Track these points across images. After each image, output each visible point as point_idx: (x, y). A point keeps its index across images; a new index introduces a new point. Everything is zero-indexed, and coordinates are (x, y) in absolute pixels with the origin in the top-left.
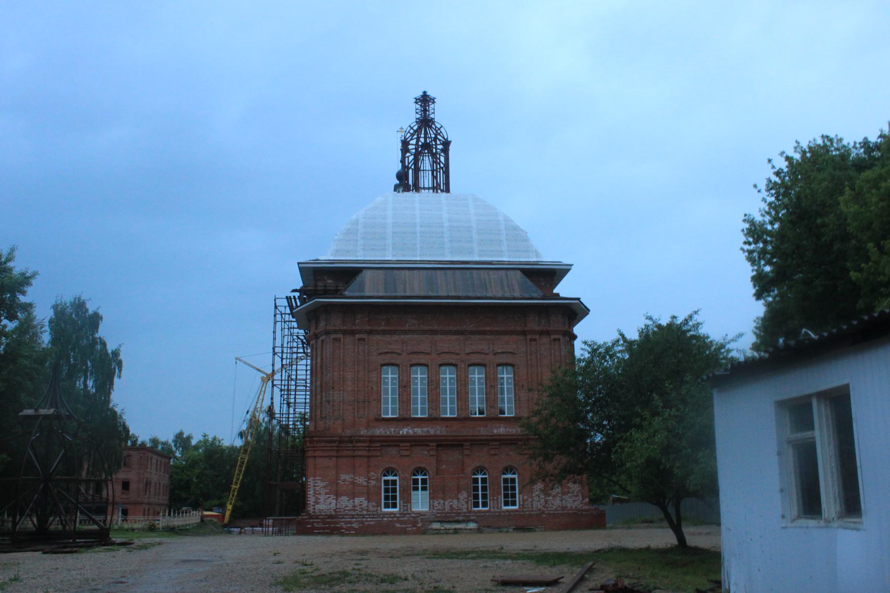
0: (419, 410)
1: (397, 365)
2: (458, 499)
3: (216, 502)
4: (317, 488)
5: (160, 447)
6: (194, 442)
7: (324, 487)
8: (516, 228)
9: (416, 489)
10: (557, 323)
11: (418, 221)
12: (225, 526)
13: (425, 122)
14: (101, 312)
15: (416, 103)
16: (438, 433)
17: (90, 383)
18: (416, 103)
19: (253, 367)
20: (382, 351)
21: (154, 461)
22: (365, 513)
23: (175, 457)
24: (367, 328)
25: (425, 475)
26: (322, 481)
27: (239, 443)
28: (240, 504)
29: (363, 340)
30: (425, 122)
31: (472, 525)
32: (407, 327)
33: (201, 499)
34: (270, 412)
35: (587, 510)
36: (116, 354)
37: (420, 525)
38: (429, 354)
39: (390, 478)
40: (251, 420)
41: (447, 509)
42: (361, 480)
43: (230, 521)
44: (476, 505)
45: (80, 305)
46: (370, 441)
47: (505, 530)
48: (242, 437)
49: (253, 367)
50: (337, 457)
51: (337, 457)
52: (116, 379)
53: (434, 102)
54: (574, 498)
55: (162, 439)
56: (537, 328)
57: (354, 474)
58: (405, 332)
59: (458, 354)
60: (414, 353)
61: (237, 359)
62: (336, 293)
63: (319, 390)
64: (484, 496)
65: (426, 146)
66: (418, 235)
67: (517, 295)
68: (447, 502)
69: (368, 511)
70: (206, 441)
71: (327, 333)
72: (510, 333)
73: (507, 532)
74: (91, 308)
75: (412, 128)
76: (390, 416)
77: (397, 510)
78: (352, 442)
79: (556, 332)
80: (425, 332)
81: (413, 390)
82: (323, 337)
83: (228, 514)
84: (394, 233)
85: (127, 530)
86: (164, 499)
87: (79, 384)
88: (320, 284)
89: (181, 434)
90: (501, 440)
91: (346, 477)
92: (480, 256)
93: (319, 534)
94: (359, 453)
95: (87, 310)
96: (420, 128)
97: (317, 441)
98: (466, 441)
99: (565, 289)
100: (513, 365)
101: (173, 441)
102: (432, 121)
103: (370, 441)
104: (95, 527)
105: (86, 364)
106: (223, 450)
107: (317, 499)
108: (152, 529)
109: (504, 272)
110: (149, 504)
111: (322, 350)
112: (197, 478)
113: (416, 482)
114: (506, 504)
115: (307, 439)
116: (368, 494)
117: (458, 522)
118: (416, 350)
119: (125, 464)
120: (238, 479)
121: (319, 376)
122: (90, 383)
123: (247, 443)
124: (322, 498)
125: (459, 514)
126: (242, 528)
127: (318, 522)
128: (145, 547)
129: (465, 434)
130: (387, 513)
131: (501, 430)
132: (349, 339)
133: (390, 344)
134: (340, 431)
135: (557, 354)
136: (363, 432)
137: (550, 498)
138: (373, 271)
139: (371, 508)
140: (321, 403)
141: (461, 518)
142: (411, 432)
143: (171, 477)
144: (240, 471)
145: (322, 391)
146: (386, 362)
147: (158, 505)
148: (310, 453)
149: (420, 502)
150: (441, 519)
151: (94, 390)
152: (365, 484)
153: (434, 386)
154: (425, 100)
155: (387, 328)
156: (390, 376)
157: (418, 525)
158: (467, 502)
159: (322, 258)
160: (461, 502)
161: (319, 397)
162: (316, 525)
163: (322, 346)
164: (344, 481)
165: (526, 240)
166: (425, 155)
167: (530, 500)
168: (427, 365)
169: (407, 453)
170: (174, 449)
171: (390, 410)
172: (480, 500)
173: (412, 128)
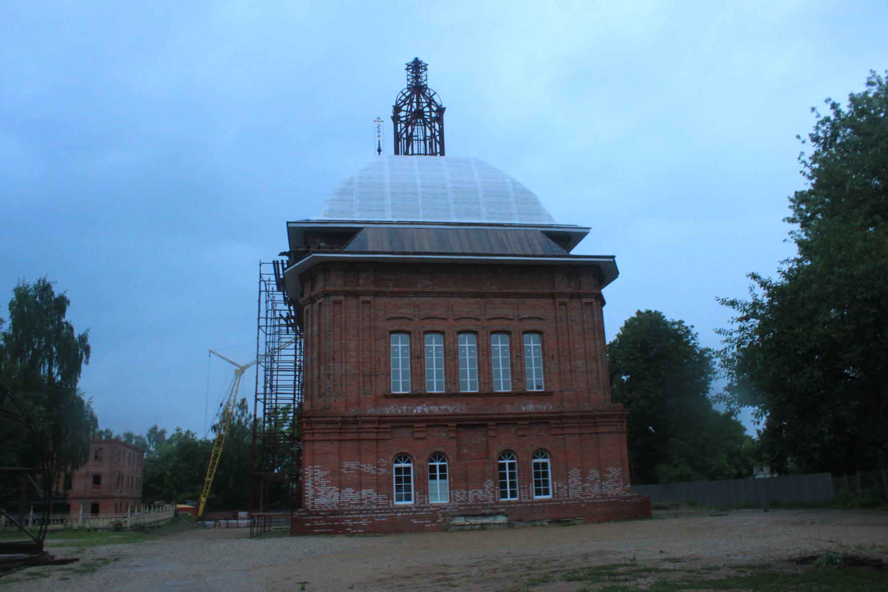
0: (435, 384)
1: (408, 333)
2: (483, 488)
3: (189, 494)
4: (317, 479)
5: (134, 442)
6: (167, 437)
7: (325, 477)
8: (525, 191)
9: (433, 477)
11: (418, 181)
12: (199, 519)
13: (418, 88)
14: (68, 296)
15: (407, 69)
16: (458, 411)
17: (55, 370)
18: (407, 69)
19: (227, 360)
20: (390, 316)
21: (127, 454)
22: (374, 507)
23: (149, 452)
25: (443, 461)
26: (322, 469)
27: (212, 436)
29: (369, 302)
30: (418, 88)
31: (501, 519)
32: (419, 288)
33: (175, 492)
34: (243, 406)
35: (629, 498)
36: (83, 338)
38: (445, 319)
39: (403, 465)
40: (223, 414)
41: (471, 500)
42: (369, 468)
43: (204, 513)
44: (504, 495)
45: (45, 288)
46: (379, 422)
47: (539, 523)
49: (227, 360)
52: (83, 366)
53: (426, 69)
54: (615, 485)
55: (137, 434)
56: (566, 290)
57: (360, 460)
58: (417, 294)
59: (478, 320)
60: (428, 318)
61: (210, 351)
63: (316, 362)
64: (513, 485)
66: (420, 196)
70: (179, 435)
71: (326, 294)
73: (542, 525)
74: (57, 291)
75: (404, 94)
76: (401, 392)
77: (411, 503)
78: (357, 423)
79: (588, 295)
80: (439, 294)
81: (427, 361)
82: (321, 300)
83: (202, 506)
84: (393, 193)
85: (89, 530)
86: (137, 492)
87: (44, 371)
89: (155, 428)
90: (531, 418)
91: (350, 465)
92: (488, 218)
93: (321, 533)
94: (366, 436)
95: (52, 293)
96: (412, 94)
97: (316, 422)
100: (540, 333)
103: (379, 422)
104: (28, 539)
105: (51, 350)
106: (196, 444)
107: (316, 491)
108: (118, 528)
110: (122, 498)
112: (171, 471)
114: (538, 493)
115: (303, 420)
117: (485, 515)
118: (430, 315)
119: (96, 457)
120: (212, 471)
122: (55, 370)
123: (220, 437)
124: (322, 490)
125: (485, 506)
126: (216, 520)
127: (318, 520)
129: (489, 412)
130: (401, 507)
131: (530, 407)
132: (352, 302)
134: (342, 410)
135: (590, 320)
136: (370, 411)
139: (381, 501)
140: (319, 377)
141: (488, 511)
142: (426, 410)
143: (144, 470)
144: (214, 463)
145: (319, 364)
146: (396, 328)
147: (130, 498)
149: (439, 494)
150: (466, 513)
151: (59, 378)
152: (374, 472)
153: (451, 357)
154: (417, 67)
155: (396, 289)
156: (400, 345)
157: (438, 522)
158: (494, 492)
159: (314, 218)
160: (486, 492)
161: (316, 370)
162: (316, 523)
163: (320, 310)
164: (349, 469)
165: (536, 202)
166: (418, 118)
167: (565, 487)
169: (423, 435)
170: (148, 443)
171: (401, 384)
172: (508, 490)
173: (404, 94)
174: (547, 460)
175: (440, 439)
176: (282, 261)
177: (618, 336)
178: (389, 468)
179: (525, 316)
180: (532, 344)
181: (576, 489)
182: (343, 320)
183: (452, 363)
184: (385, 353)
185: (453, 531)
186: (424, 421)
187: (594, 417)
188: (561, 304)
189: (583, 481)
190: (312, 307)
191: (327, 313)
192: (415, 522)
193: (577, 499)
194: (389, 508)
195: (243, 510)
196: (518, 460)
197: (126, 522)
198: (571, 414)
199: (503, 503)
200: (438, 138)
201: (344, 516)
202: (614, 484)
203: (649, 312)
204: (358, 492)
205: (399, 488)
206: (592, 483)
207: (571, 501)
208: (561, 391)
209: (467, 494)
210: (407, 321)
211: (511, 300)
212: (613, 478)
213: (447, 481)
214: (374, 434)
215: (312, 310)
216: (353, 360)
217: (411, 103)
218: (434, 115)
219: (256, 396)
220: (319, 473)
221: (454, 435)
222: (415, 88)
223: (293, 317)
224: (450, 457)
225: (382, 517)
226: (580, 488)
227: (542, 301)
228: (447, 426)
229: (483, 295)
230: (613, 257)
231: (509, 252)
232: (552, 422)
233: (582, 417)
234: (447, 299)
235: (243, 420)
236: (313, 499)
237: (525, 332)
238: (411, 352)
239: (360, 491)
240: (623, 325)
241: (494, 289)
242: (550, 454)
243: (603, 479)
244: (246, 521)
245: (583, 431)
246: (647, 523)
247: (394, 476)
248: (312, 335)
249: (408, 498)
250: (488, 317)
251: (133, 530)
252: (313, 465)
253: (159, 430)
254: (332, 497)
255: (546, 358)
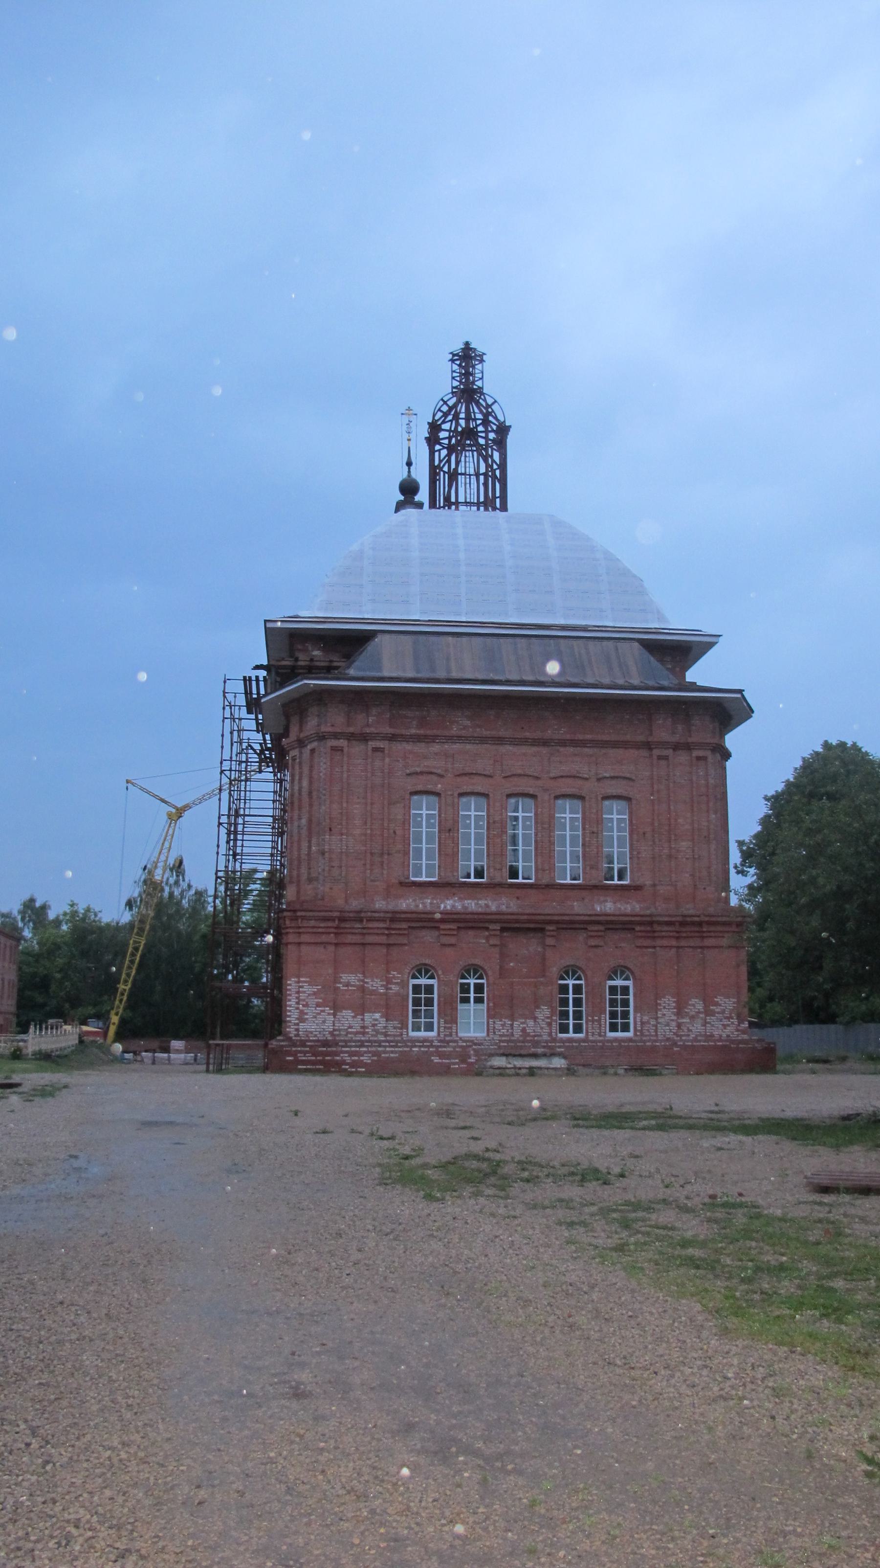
2: (535, 1019)
3: (91, 1010)
6: (51, 915)
7: (315, 994)
9: (466, 1000)
10: (701, 730)
11: (462, 556)
13: (468, 392)
15: (452, 361)
18: (452, 361)
19: (155, 796)
20: (412, 770)
22: (382, 1038)
24: (389, 730)
25: (481, 977)
27: (126, 917)
28: (130, 1014)
30: (468, 392)
31: (558, 1063)
32: (455, 730)
33: (67, 1005)
37: (472, 1060)
39: (423, 981)
41: (517, 1034)
42: (376, 984)
44: (564, 1029)
47: (612, 1071)
48: (131, 909)
49: (155, 796)
50: (336, 945)
51: (336, 945)
53: (482, 361)
54: (726, 1022)
57: (363, 973)
58: (451, 739)
59: (537, 778)
60: (465, 774)
61: (128, 782)
62: (328, 671)
63: (304, 832)
64: (578, 1015)
65: (470, 433)
67: (635, 682)
68: (516, 1024)
69: (386, 1035)
70: (74, 914)
71: (322, 737)
72: (625, 745)
73: (616, 1074)
75: (445, 403)
76: (424, 879)
77: (432, 1034)
78: (361, 920)
79: (701, 746)
80: (483, 740)
81: (448, 832)
88: (301, 656)
89: (32, 900)
91: (351, 978)
96: (458, 402)
98: (550, 922)
99: (703, 674)
100: (628, 799)
101: (19, 912)
102: (480, 391)
103: (392, 920)
107: (302, 1013)
109: (610, 644)
111: (311, 767)
113: (465, 988)
114: (613, 1028)
116: (387, 1006)
117: (535, 1056)
121: (306, 809)
124: (310, 1012)
125: (536, 1044)
127: (305, 1053)
128: (46, 1092)
129: (547, 911)
131: (608, 906)
132: (358, 749)
133: (426, 757)
134: (340, 902)
136: (380, 904)
137: (686, 1020)
138: (393, 636)
139: (391, 1031)
141: (540, 1051)
142: (459, 906)
143: (20, 969)
144: (132, 962)
146: (420, 788)
148: (291, 938)
149: (473, 1023)
154: (467, 357)
155: (422, 732)
157: (470, 1063)
158: (550, 1024)
159: (304, 613)
160: (540, 1023)
161: (304, 845)
162: (302, 1058)
164: (348, 984)
166: (468, 438)
168: (485, 795)
169: (453, 940)
170: (20, 925)
174: (629, 983)
175: (478, 946)
176: (257, 677)
177: (788, 784)
178: (404, 984)
179: (607, 775)
180: (616, 816)
181: (668, 1025)
182: (345, 775)
183: (499, 840)
184: (404, 823)
185: (488, 1076)
186: (454, 921)
187: (700, 924)
188: (660, 758)
189: (679, 1013)
190: (301, 753)
191: (323, 765)
192: (436, 1060)
193: (668, 1039)
194: (402, 1041)
195: (177, 1037)
196: (586, 980)
197: (26, 1047)
198: (666, 919)
199: (562, 1041)
200: (498, 473)
201: (339, 1049)
202: (722, 1020)
203: (842, 745)
204: (360, 1017)
205: (416, 1014)
206: (692, 1018)
207: (661, 1041)
208: (654, 885)
209: (512, 1025)
210: (435, 778)
211: (586, 750)
212: (723, 1012)
213: (484, 1007)
214: (385, 937)
215: (300, 757)
216: (357, 832)
217: (456, 417)
218: (492, 436)
219: (216, 874)
220: (307, 989)
221: (498, 943)
222: (463, 391)
223: (268, 749)
224: (490, 973)
225: (392, 1052)
226: (674, 1024)
227: (633, 753)
228: (487, 929)
229: (545, 743)
230: (740, 691)
231: (590, 680)
232: (638, 928)
233: (683, 924)
234: (495, 747)
235: (177, 893)
236: (297, 1024)
237: (606, 798)
238: (440, 822)
239: (363, 1015)
240: (799, 763)
241: (562, 733)
242: (632, 973)
243: (708, 1013)
244: (182, 1056)
245: (683, 943)
246: (768, 1078)
247: (411, 996)
248: (300, 794)
249: (429, 1027)
250: (552, 775)
251: (36, 1059)
252: (298, 976)
253: (38, 905)
254: (324, 1022)
255: (635, 837)
